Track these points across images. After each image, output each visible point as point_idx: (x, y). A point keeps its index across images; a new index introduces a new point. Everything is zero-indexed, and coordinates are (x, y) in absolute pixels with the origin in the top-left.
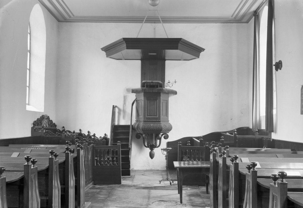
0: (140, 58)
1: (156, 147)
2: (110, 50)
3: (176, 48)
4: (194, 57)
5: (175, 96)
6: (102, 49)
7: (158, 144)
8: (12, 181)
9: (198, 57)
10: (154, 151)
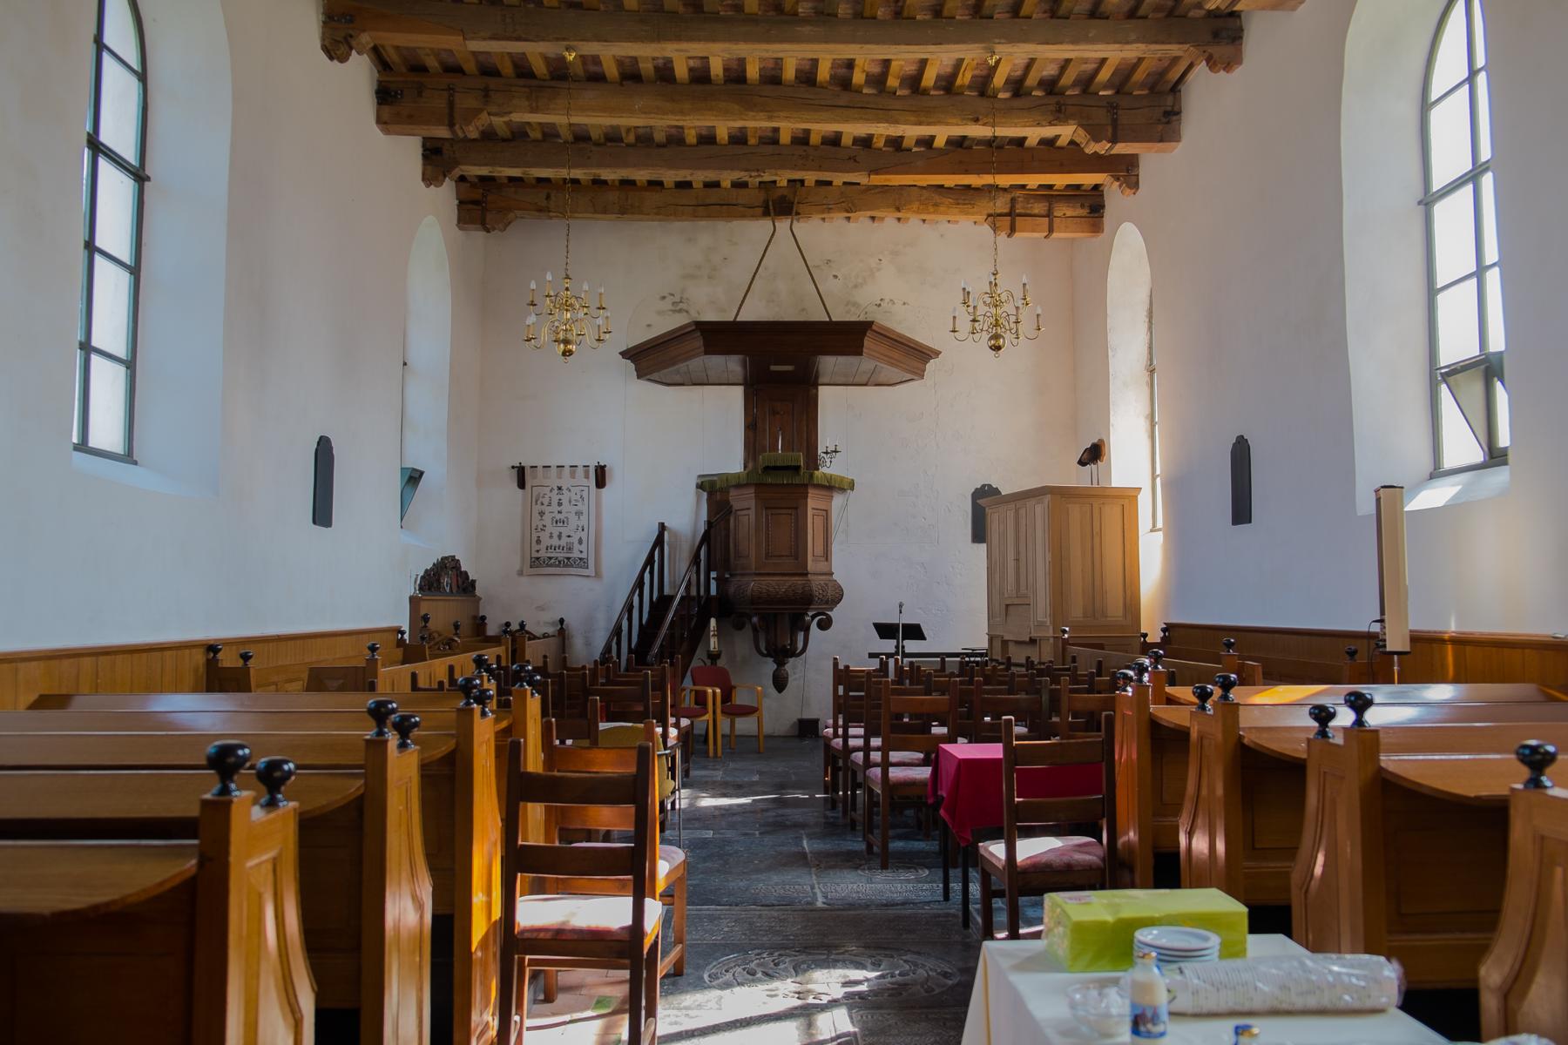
0: (740, 379)
1: (793, 653)
2: (651, 359)
3: (857, 351)
4: (910, 376)
5: (908, 395)
6: (624, 354)
7: (800, 645)
8: (161, 884)
9: (921, 374)
10: (788, 667)
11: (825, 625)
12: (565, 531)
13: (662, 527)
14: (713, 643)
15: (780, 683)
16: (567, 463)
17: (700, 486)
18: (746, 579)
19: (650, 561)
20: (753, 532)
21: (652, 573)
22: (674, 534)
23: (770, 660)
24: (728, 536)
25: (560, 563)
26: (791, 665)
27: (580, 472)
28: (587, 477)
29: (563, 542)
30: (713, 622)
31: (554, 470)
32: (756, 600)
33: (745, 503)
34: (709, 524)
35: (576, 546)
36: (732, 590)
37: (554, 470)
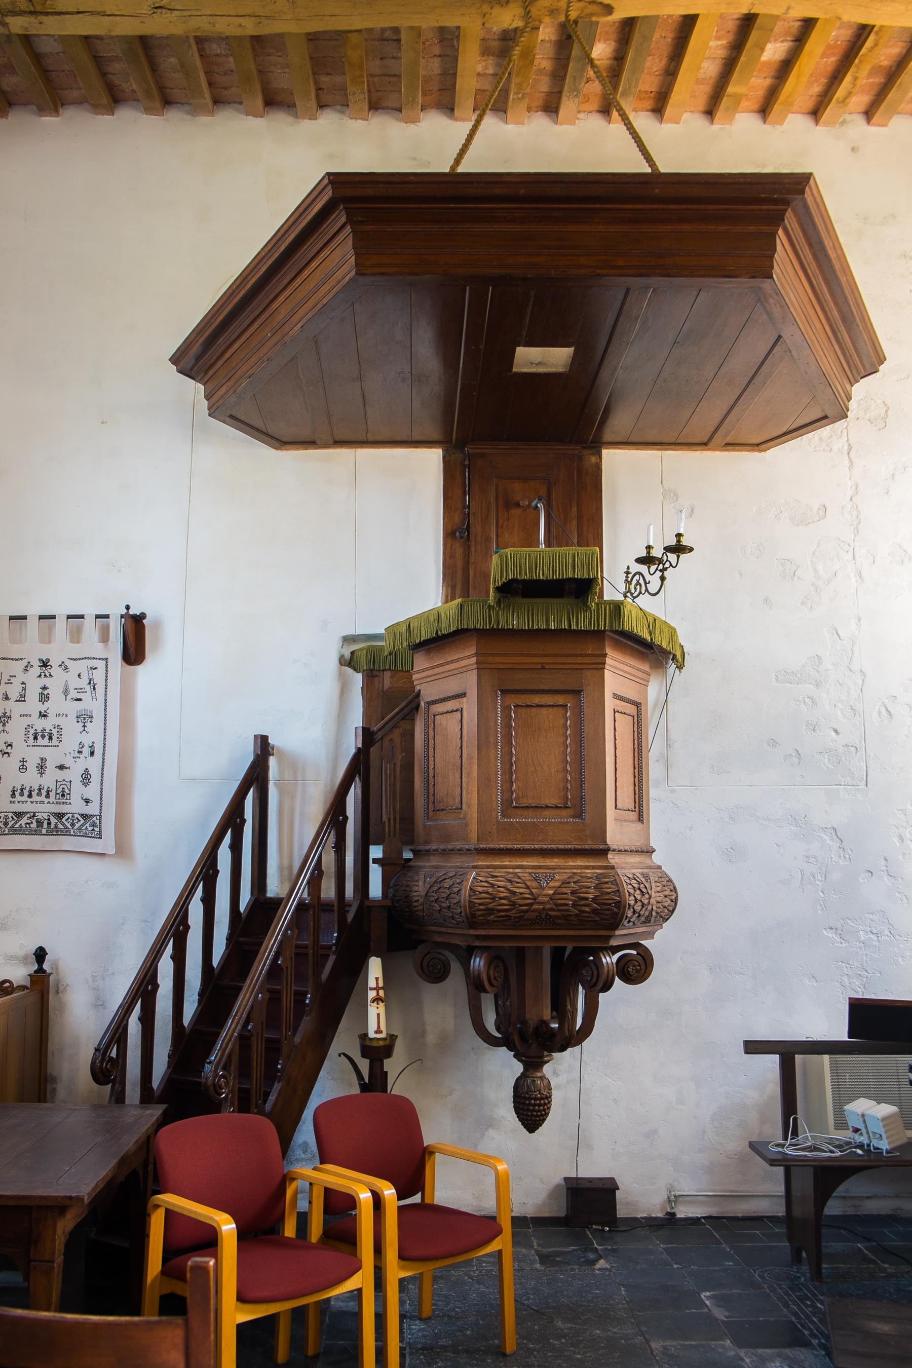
0: (436, 435)
1: (571, 1038)
11: (637, 968)
12: (53, 756)
13: (264, 747)
14: (376, 1019)
15: (531, 1108)
16: (61, 610)
17: (350, 662)
18: (457, 861)
19: (232, 819)
20: (471, 750)
21: (236, 848)
22: (292, 763)
23: (504, 1055)
24: (409, 766)
25: (39, 826)
26: (560, 1069)
27: (90, 627)
28: (105, 638)
29: (49, 780)
30: (375, 968)
31: (33, 625)
32: (480, 916)
33: (454, 692)
34: (367, 734)
35: (77, 790)
36: (420, 888)
37: (33, 625)
